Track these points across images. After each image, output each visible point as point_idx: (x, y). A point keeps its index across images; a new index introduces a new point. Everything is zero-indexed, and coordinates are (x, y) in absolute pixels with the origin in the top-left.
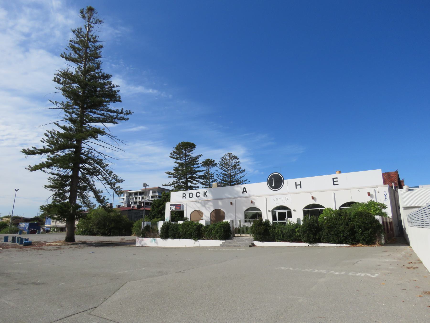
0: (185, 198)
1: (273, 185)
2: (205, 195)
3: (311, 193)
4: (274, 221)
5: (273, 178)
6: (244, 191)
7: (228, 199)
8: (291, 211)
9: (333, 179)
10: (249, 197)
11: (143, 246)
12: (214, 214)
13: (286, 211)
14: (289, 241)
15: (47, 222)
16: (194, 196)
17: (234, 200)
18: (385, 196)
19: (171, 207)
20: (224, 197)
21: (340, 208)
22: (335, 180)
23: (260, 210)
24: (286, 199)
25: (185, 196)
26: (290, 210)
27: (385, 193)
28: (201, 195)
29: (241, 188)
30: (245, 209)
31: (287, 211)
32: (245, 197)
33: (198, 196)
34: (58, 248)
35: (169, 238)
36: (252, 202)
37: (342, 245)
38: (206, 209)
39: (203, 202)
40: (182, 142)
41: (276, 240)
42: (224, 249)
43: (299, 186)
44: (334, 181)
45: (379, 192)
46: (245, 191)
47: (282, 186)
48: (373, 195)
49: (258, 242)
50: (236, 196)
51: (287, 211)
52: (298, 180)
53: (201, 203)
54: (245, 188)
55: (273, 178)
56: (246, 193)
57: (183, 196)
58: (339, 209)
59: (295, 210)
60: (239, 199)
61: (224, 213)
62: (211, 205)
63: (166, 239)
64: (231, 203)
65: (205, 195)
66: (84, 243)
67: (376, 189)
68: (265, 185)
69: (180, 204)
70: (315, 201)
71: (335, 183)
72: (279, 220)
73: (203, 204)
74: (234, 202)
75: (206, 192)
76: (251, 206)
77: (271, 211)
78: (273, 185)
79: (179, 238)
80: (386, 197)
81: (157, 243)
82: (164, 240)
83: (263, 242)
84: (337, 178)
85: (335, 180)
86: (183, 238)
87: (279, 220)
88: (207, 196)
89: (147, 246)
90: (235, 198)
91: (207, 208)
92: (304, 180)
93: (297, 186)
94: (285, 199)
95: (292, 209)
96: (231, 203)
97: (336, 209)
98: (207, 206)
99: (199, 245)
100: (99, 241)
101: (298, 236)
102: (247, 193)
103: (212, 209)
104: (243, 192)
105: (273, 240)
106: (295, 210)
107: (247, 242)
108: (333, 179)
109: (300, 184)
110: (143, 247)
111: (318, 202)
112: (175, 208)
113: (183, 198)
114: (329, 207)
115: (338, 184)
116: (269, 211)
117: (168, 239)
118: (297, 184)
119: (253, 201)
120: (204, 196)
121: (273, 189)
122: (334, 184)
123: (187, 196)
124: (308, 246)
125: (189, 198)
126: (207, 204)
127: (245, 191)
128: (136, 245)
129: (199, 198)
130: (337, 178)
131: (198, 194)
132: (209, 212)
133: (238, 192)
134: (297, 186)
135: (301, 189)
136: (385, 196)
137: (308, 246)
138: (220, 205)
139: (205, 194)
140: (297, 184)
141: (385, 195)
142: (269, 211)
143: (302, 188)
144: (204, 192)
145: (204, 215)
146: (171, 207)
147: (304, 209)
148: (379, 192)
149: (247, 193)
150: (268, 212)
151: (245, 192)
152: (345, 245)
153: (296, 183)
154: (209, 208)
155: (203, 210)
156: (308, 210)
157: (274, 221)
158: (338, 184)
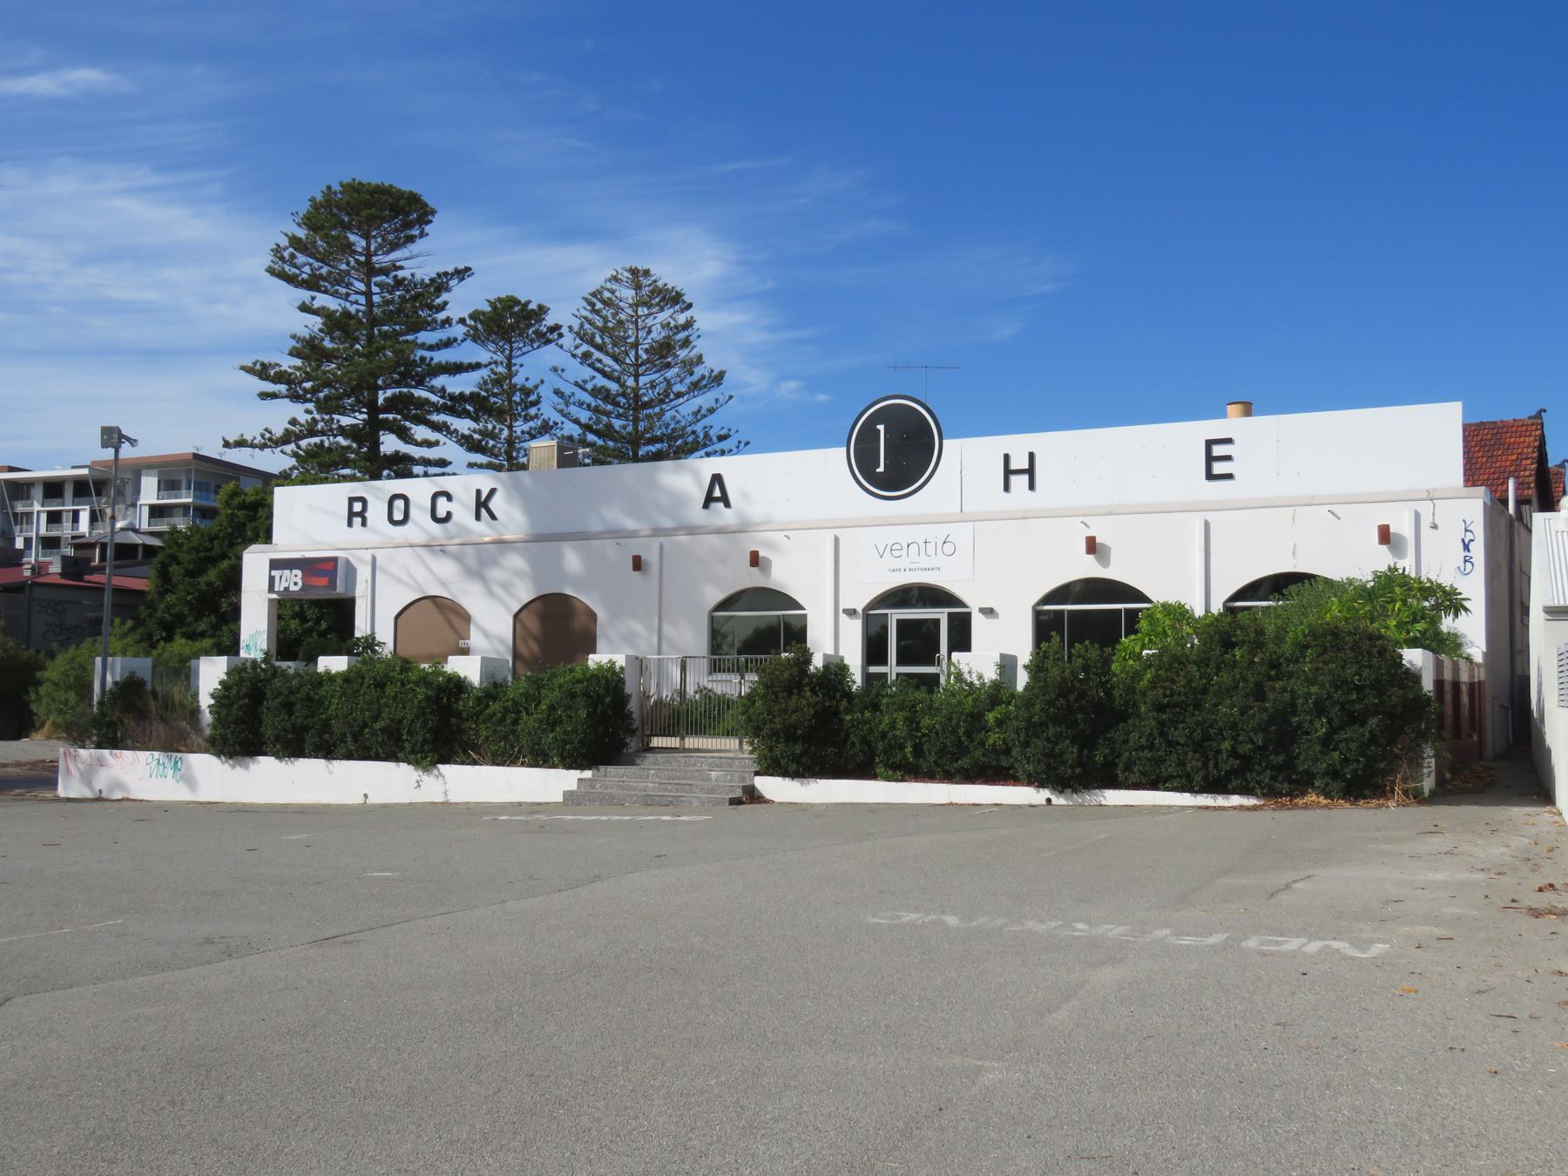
0: (364, 524)
1: (881, 469)
2: (483, 512)
4: (873, 669)
5: (881, 428)
6: (716, 493)
7: (618, 541)
8: (970, 613)
9: (1210, 444)
10: (744, 528)
12: (533, 623)
13: (942, 614)
16: (420, 515)
17: (656, 542)
18: (1466, 547)
19: (274, 573)
20: (595, 526)
22: (1218, 450)
23: (800, 607)
24: (948, 548)
25: (362, 514)
27: (1466, 530)
28: (462, 511)
29: (696, 475)
30: (717, 596)
32: (720, 531)
33: (441, 513)
36: (755, 559)
37: (1221, 801)
38: (491, 593)
41: (880, 769)
42: (572, 817)
44: (1210, 459)
45: (1435, 527)
46: (717, 493)
49: (779, 779)
50: (667, 523)
51: (949, 613)
52: (1018, 446)
53: (458, 558)
54: (717, 479)
55: (881, 428)
56: (721, 504)
59: (989, 612)
60: (683, 539)
61: (592, 616)
63: (248, 759)
65: (483, 512)
67: (1425, 509)
68: (834, 462)
71: (1218, 468)
73: (472, 562)
74: (651, 556)
75: (493, 492)
78: (881, 469)
79: (328, 750)
80: (1467, 553)
81: (190, 781)
82: (233, 767)
83: (806, 781)
84: (1229, 441)
85: (1218, 450)
88: (493, 517)
90: (658, 532)
91: (498, 590)
92: (1051, 446)
93: (1014, 479)
95: (973, 600)
96: (638, 564)
97: (1207, 611)
98: (495, 574)
101: (995, 751)
102: (727, 505)
103: (525, 594)
104: (709, 500)
105: (863, 771)
106: (989, 612)
107: (716, 780)
108: (1210, 444)
111: (1115, 572)
113: (350, 524)
115: (1229, 476)
116: (851, 613)
117: (261, 758)
119: (761, 554)
120: (478, 517)
122: (1210, 476)
124: (1044, 802)
126: (494, 562)
127: (717, 493)
128: (62, 792)
129: (449, 525)
130: (1229, 441)
131: (442, 501)
132: (506, 607)
133: (679, 500)
134: (1014, 479)
136: (1466, 547)
137: (1049, 801)
139: (482, 504)
141: (1463, 540)
142: (851, 613)
144: (479, 492)
148: (1435, 527)
149: (727, 505)
151: (717, 500)
153: (1007, 458)
154: (506, 586)
155: (472, 599)
157: (873, 669)
158: (1229, 476)
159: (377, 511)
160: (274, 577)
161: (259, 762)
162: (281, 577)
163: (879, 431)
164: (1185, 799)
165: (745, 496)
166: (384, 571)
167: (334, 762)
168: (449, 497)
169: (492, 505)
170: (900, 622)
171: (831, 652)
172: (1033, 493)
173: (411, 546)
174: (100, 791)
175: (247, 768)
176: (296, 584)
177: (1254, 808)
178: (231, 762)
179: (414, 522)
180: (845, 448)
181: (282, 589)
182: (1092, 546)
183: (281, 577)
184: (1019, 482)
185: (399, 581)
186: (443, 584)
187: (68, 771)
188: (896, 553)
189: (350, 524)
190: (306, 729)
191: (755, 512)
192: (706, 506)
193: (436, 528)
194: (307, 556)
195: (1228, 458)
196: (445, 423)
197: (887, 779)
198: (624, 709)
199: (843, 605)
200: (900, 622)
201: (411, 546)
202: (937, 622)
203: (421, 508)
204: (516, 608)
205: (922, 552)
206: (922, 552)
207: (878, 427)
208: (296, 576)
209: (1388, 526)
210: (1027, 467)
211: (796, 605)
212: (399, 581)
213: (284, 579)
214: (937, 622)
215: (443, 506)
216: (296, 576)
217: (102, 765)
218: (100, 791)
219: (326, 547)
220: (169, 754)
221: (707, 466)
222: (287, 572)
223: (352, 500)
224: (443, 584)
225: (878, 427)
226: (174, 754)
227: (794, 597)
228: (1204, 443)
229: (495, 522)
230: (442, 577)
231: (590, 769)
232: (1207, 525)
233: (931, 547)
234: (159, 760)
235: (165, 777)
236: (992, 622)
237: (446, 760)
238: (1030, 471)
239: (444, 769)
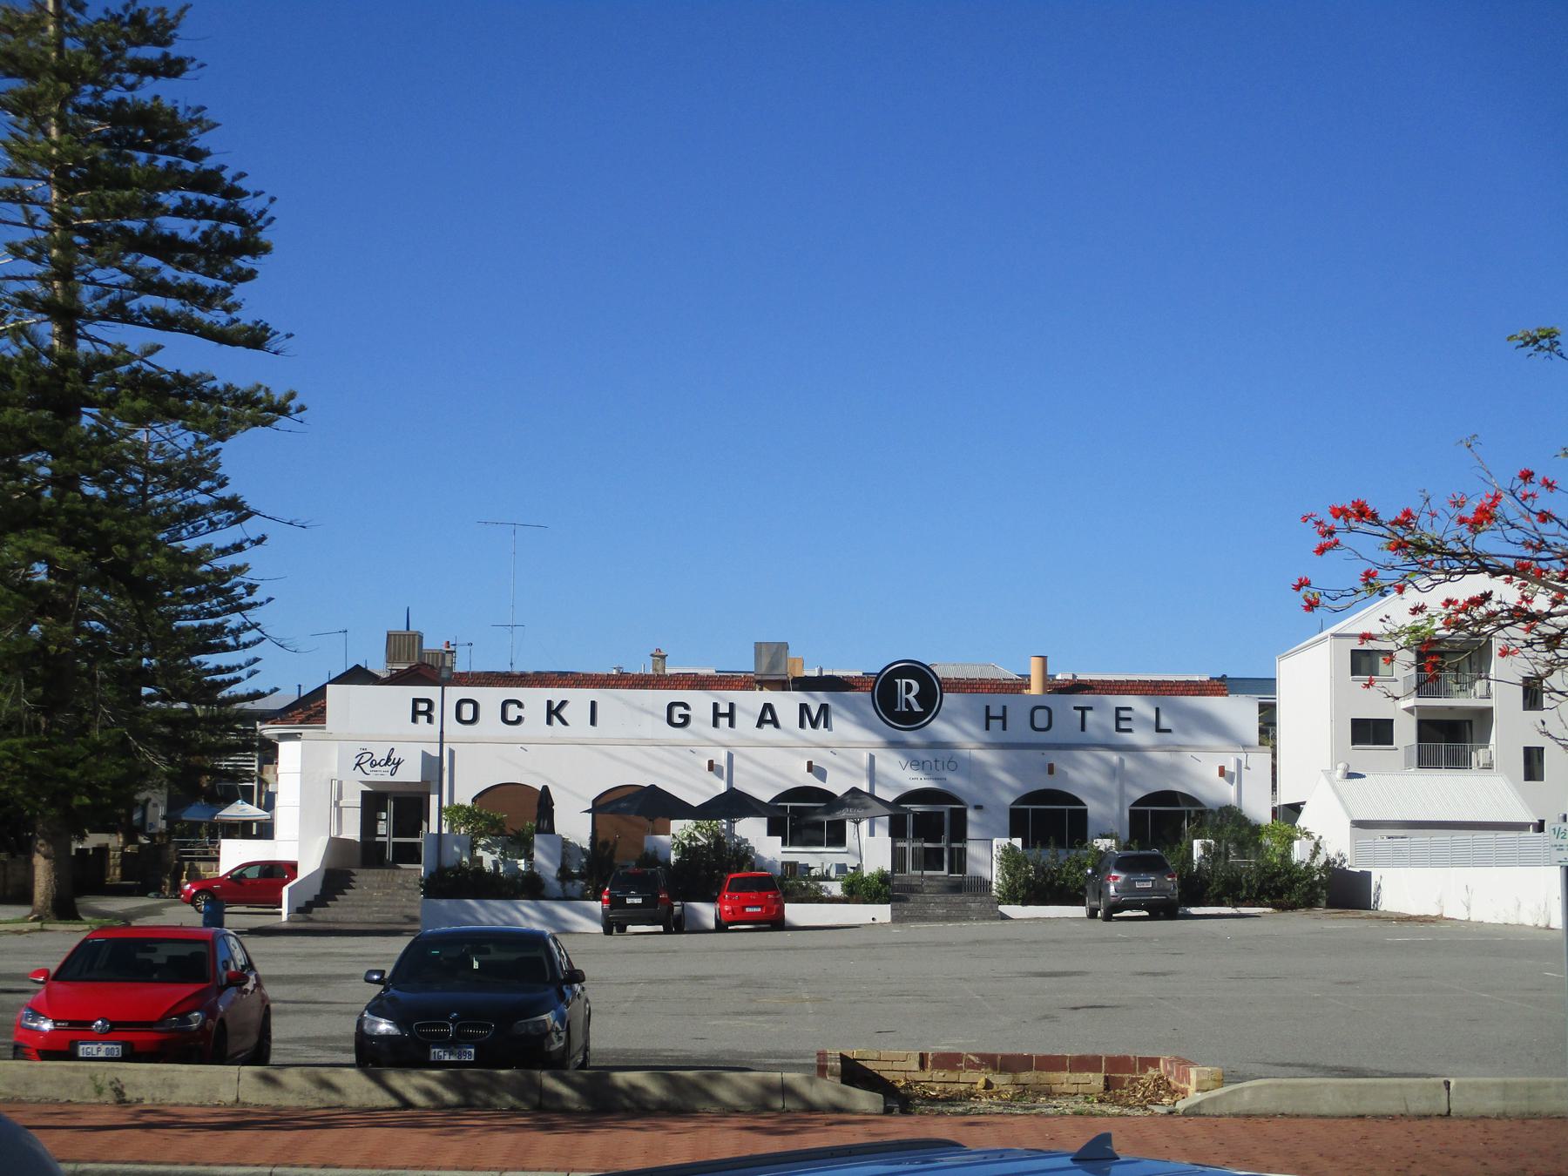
0: (731, 724)
2: (555, 719)
9: (1118, 709)
13: (945, 809)
15: (1175, 770)
30: (1139, 794)
33: (512, 716)
34: (385, 958)
40: (1483, 592)
43: (1000, 722)
44: (1118, 719)
46: (769, 717)
47: (885, 718)
54: (768, 707)
57: (416, 714)
65: (555, 719)
71: (1123, 725)
75: (563, 703)
84: (1129, 709)
85: (1123, 714)
88: (564, 723)
93: (992, 722)
94: (946, 763)
100: (6, 972)
102: (777, 725)
104: (761, 722)
109: (1001, 715)
118: (1000, 721)
121: (894, 721)
122: (1118, 729)
125: (1030, 729)
127: (769, 717)
131: (512, 709)
134: (992, 722)
140: (1000, 721)
144: (550, 703)
148: (1247, 768)
149: (777, 725)
151: (768, 722)
153: (988, 708)
156: (1147, 811)
157: (115, 874)
159: (746, 721)
163: (897, 683)
168: (520, 705)
169: (563, 713)
172: (416, 725)
184: (724, 721)
189: (414, 720)
192: (759, 725)
198: (502, 878)
209: (1223, 767)
210: (728, 712)
219: (622, 742)
223: (416, 701)
227: (1157, 790)
233: (939, 765)
238: (1003, 718)
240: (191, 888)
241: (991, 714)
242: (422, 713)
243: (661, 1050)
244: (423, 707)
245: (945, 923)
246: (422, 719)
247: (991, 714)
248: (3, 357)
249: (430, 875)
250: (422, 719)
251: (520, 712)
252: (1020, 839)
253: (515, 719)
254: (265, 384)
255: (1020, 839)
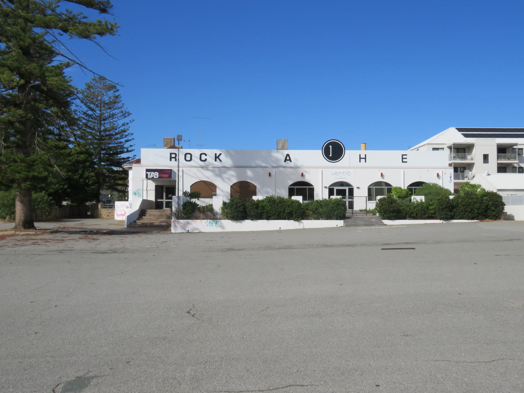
1: (331, 156)
2: (217, 159)
3: (310, 169)
5: (331, 146)
6: (288, 158)
7: (262, 169)
8: (353, 188)
9: (403, 155)
10: (296, 168)
11: (189, 231)
12: (237, 189)
13: (347, 188)
14: (422, 218)
16: (196, 160)
17: (274, 170)
18: (451, 178)
19: (147, 173)
20: (254, 165)
21: (369, 187)
22: (404, 157)
23: (313, 186)
24: (349, 174)
25: (175, 158)
26: (352, 187)
28: (210, 159)
29: (283, 154)
30: (291, 183)
31: (349, 188)
32: (291, 168)
35: (291, 220)
36: (302, 175)
37: (473, 221)
38: (224, 180)
39: (216, 169)
41: (408, 218)
44: (403, 158)
45: (445, 174)
46: (288, 158)
48: (440, 176)
49: (388, 220)
50: (275, 165)
51: (349, 188)
52: (363, 153)
53: (212, 171)
54: (288, 155)
55: (331, 146)
56: (289, 161)
57: (171, 158)
58: (407, 188)
59: (358, 188)
60: (282, 169)
61: (255, 187)
62: (232, 176)
63: (242, 221)
64: (270, 174)
65: (217, 159)
66: (44, 231)
67: (444, 170)
68: (319, 154)
69: (171, 170)
70: (382, 178)
71: (404, 160)
72: (166, 199)
73: (217, 173)
75: (220, 154)
76: (301, 179)
77: (328, 187)
78: (331, 156)
79: (268, 218)
81: (222, 227)
82: (237, 223)
83: (394, 220)
84: (406, 155)
85: (404, 157)
86: (275, 219)
87: (166, 199)
88: (221, 161)
89: (201, 232)
90: (274, 167)
92: (371, 154)
93: (361, 160)
94: (347, 173)
95: (355, 186)
96: (270, 174)
98: (225, 176)
99: (304, 227)
101: (432, 214)
103: (235, 181)
104: (286, 160)
105: (404, 218)
106: (358, 188)
108: (403, 155)
109: (364, 157)
110: (201, 233)
111: (386, 180)
112: (158, 176)
113: (171, 160)
114: (398, 186)
115: (406, 162)
116: (326, 187)
119: (303, 174)
120: (216, 160)
122: (403, 162)
123: (181, 157)
126: (225, 173)
128: (173, 230)
129: (206, 162)
130: (406, 155)
132: (229, 184)
133: (277, 160)
134: (361, 160)
135: (171, 162)
136: (451, 178)
138: (249, 176)
139: (217, 157)
142: (326, 187)
143: (361, 162)
144: (216, 154)
145: (218, 188)
146: (149, 173)
147: (370, 185)
148: (445, 174)
149: (291, 161)
150: (324, 188)
151: (288, 160)
152: (475, 221)
154: (229, 179)
155: (217, 181)
158: (406, 162)
159: (181, 157)
160: (148, 174)
161: (245, 221)
162: (150, 174)
164: (466, 221)
165: (296, 160)
166: (187, 174)
167: (270, 221)
168: (206, 155)
170: (337, 190)
171: (102, 194)
173: (196, 167)
174: (188, 231)
175: (241, 223)
176: (156, 176)
177: (479, 222)
178: (236, 222)
179: (194, 161)
180: (321, 151)
181: (151, 177)
182: (382, 175)
183: (150, 174)
185: (192, 176)
186: (208, 178)
187: (175, 226)
188: (336, 175)
189: (171, 160)
190: (263, 213)
191: (299, 164)
192: (285, 161)
193: (202, 163)
194: (157, 169)
195: (406, 158)
196: (466, 136)
197: (409, 219)
199: (324, 185)
200: (337, 190)
201: (196, 167)
202: (345, 190)
203: (196, 157)
204: (232, 184)
205: (343, 175)
206: (343, 175)
207: (330, 146)
208: (156, 174)
211: (312, 186)
212: (192, 176)
213: (151, 175)
214: (345, 190)
215: (203, 157)
216: (156, 174)
217: (188, 224)
218: (188, 231)
220: (214, 220)
221: (286, 152)
222: (152, 173)
223: (171, 154)
224: (208, 178)
225: (330, 146)
226: (215, 220)
228: (483, 155)
229: (221, 162)
230: (207, 176)
231: (343, 220)
232: (322, 171)
234: (210, 222)
235: (213, 226)
236: (359, 190)
237: (303, 219)
239: (303, 221)
240: (68, 188)
241: (361, 157)
242: (173, 158)
243: (100, 236)
244: (173, 156)
245: (370, 227)
246: (173, 160)
247: (361, 157)
248: (2, 95)
249: (271, 197)
250: (173, 160)
251: (206, 157)
252: (301, 197)
253: (204, 159)
254: (121, 92)
255: (301, 197)
